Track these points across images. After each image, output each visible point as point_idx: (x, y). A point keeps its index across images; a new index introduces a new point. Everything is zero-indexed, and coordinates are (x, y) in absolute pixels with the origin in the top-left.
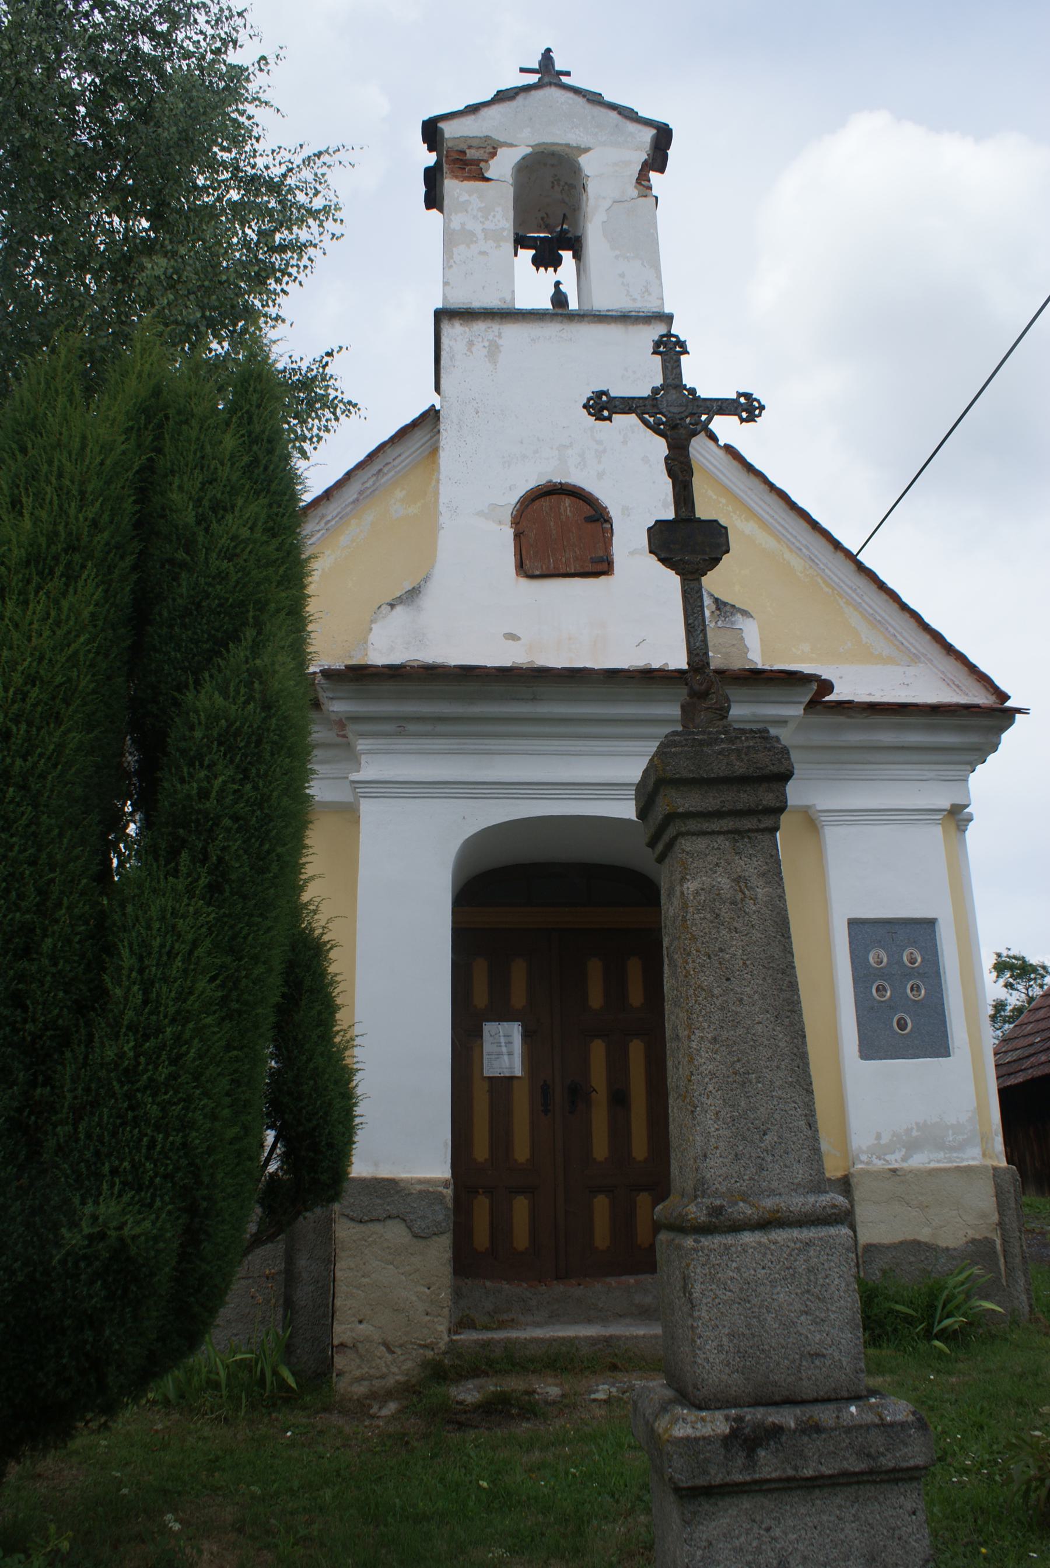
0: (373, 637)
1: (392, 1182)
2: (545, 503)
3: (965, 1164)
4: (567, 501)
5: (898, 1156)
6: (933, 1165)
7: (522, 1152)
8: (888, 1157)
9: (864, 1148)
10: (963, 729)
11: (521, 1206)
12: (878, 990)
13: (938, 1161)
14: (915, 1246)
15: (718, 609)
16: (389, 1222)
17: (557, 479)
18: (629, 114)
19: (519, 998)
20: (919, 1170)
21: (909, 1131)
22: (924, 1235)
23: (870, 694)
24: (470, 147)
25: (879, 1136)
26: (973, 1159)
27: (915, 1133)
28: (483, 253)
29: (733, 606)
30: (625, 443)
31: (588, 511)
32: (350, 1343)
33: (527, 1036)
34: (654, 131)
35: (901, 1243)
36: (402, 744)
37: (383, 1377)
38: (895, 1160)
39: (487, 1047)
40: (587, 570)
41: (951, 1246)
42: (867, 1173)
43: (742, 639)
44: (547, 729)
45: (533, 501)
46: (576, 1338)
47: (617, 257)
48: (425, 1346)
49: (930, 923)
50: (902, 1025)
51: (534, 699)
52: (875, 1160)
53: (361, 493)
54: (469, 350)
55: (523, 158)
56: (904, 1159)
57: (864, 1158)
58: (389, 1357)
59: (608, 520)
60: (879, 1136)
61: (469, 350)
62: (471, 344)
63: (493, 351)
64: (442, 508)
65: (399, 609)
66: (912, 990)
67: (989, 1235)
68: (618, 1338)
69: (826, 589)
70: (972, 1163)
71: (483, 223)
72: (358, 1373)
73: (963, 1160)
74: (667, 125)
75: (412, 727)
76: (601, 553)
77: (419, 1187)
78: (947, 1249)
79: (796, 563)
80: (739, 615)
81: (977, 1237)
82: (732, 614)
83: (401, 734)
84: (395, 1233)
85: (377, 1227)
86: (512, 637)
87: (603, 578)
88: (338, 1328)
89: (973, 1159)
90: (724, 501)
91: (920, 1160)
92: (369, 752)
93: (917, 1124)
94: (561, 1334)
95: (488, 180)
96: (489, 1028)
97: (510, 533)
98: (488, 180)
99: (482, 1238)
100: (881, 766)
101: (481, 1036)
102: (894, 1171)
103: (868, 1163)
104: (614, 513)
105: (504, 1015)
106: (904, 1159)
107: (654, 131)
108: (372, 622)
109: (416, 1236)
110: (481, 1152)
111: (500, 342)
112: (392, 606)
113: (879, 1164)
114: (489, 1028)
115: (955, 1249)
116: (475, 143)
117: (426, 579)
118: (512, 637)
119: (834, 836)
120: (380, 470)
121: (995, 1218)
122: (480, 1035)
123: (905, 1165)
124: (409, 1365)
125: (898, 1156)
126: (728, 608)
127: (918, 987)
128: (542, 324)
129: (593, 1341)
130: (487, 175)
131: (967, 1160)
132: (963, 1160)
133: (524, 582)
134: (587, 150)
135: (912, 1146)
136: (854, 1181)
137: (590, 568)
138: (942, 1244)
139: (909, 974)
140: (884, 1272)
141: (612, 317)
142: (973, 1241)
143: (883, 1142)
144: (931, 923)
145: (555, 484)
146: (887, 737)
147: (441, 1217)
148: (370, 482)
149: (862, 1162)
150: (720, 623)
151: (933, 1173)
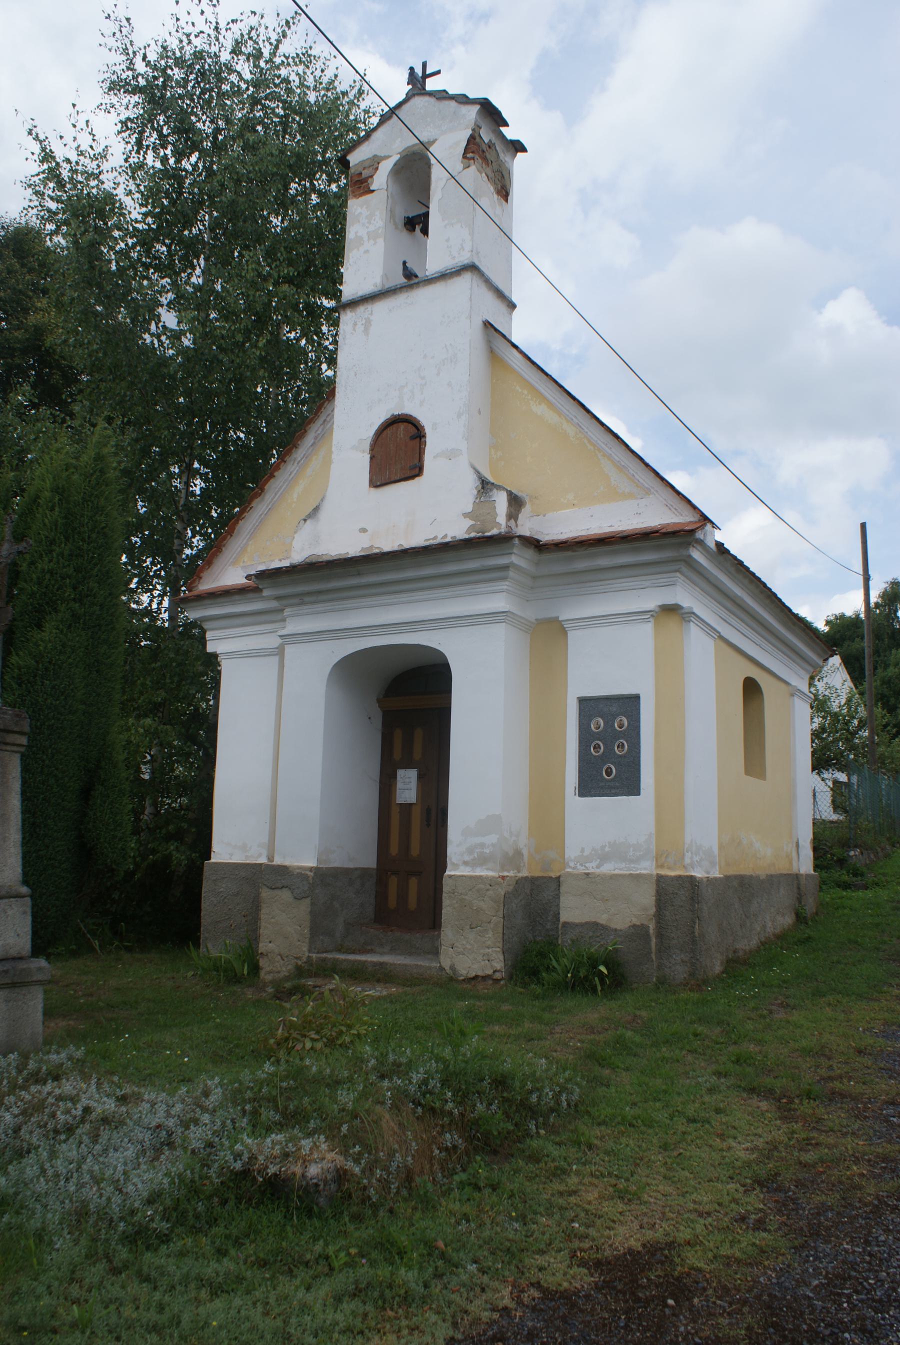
0: (294, 543)
1: (285, 868)
2: (389, 431)
3: (638, 872)
4: (402, 426)
5: (594, 864)
6: (617, 872)
7: (415, 851)
8: (587, 865)
9: (573, 858)
10: (660, 548)
11: (413, 882)
12: (594, 748)
13: (620, 869)
14: (595, 926)
15: (483, 488)
16: (284, 890)
17: (396, 413)
18: (463, 99)
19: (417, 754)
20: (604, 875)
21: (603, 847)
22: (603, 919)
23: (611, 526)
24: (364, 169)
25: (583, 850)
26: (645, 869)
27: (607, 849)
28: (367, 252)
29: (493, 484)
30: (438, 374)
31: (413, 430)
32: (265, 953)
33: (420, 777)
34: (478, 107)
35: (587, 923)
36: (306, 609)
37: (279, 972)
38: (591, 867)
39: (400, 785)
40: (407, 475)
41: (618, 927)
42: (570, 874)
43: (495, 507)
44: (374, 591)
45: (384, 430)
46: (366, 961)
47: (445, 226)
48: (296, 958)
49: (636, 699)
50: (609, 772)
51: (359, 574)
52: (579, 866)
53: (316, 438)
54: (354, 330)
55: (395, 165)
56: (598, 867)
57: (572, 864)
58: (282, 962)
59: (424, 436)
60: (583, 850)
61: (354, 330)
62: (355, 324)
63: (368, 324)
64: (334, 449)
65: (308, 522)
66: (618, 747)
67: (646, 923)
68: (386, 964)
69: (590, 447)
70: (643, 872)
71: (367, 227)
72: (268, 969)
73: (637, 869)
74: (486, 99)
75: (307, 599)
76: (416, 462)
77: (298, 871)
78: (616, 930)
79: (571, 430)
80: (495, 490)
81: (638, 923)
82: (491, 490)
83: (303, 603)
84: (286, 895)
85: (278, 892)
86: (364, 530)
87: (417, 479)
88: (261, 945)
89: (645, 869)
90: (526, 392)
91: (608, 868)
92: (289, 616)
93: (609, 843)
94: (369, 959)
95: (373, 191)
96: (401, 773)
97: (367, 457)
98: (373, 191)
99: (392, 903)
100: (592, 584)
101: (396, 778)
102: (587, 874)
103: (574, 868)
104: (428, 430)
105: (408, 764)
106: (598, 867)
107: (478, 107)
108: (295, 532)
109: (295, 898)
110: (394, 849)
111: (372, 318)
112: (305, 520)
113: (581, 869)
114: (401, 773)
115: (621, 930)
116: (366, 164)
117: (322, 500)
118: (364, 530)
119: (574, 637)
120: (325, 421)
121: (653, 910)
122: (395, 777)
123: (598, 871)
124: (290, 967)
125: (594, 864)
126: (489, 486)
127: (623, 744)
128: (396, 297)
129: (375, 964)
130: (372, 188)
131: (641, 869)
132: (637, 869)
133: (373, 490)
134: (434, 142)
135: (604, 858)
136: (561, 879)
137: (408, 474)
138: (613, 925)
139: (616, 736)
140: (573, 941)
141: (435, 278)
142: (634, 926)
143: (585, 854)
144: (636, 699)
145: (396, 416)
146: (604, 562)
147: (306, 888)
148: (321, 430)
149: (570, 867)
150: (482, 499)
151: (613, 877)
